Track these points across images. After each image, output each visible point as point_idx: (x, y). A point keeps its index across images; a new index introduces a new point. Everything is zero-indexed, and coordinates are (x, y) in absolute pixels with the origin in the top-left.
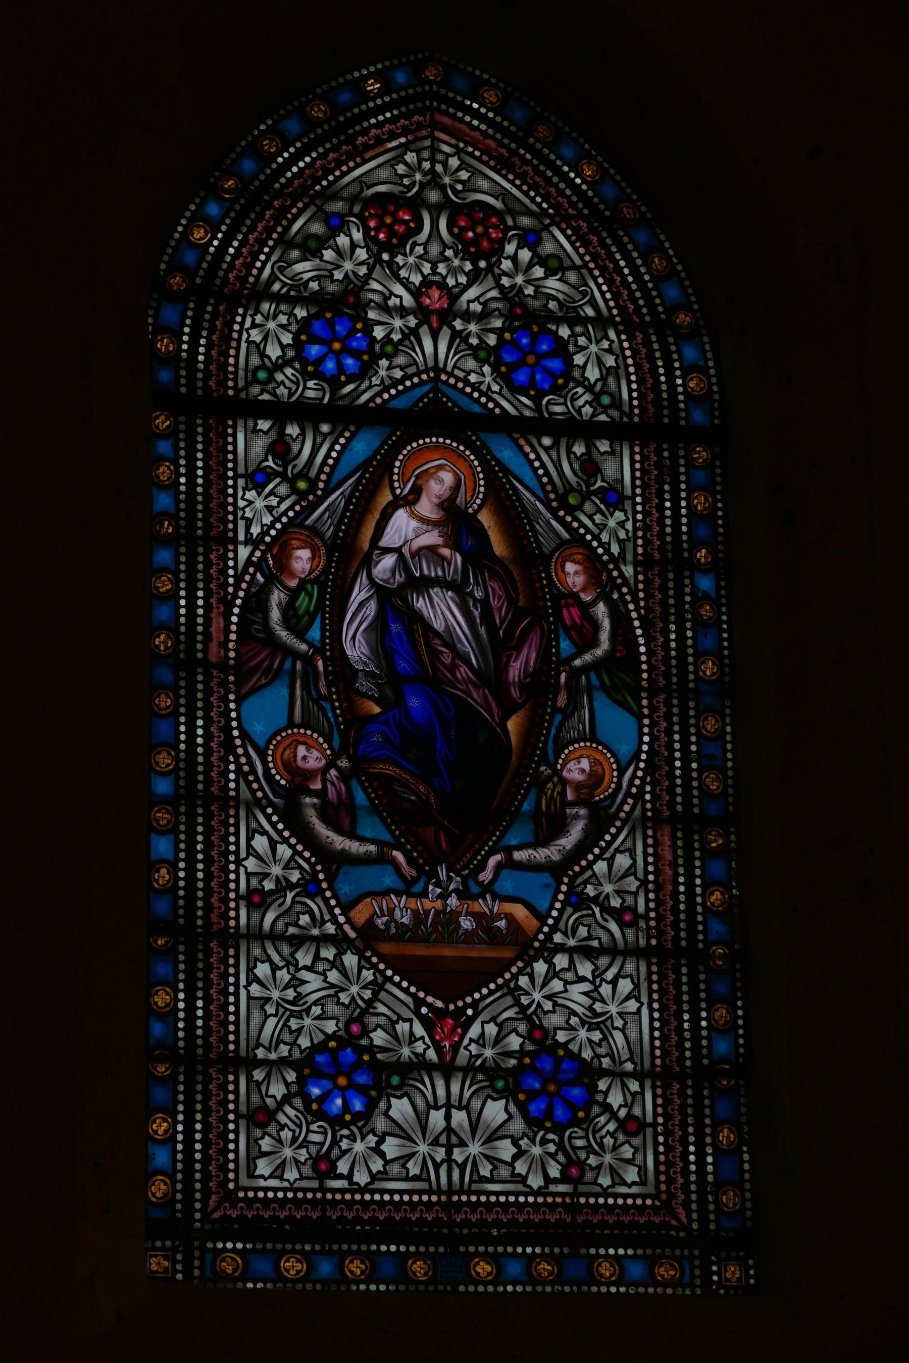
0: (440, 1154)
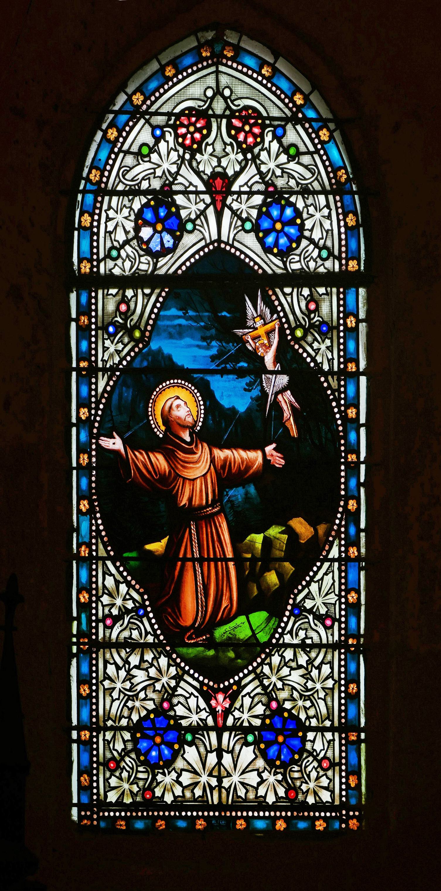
0: (214, 782)
